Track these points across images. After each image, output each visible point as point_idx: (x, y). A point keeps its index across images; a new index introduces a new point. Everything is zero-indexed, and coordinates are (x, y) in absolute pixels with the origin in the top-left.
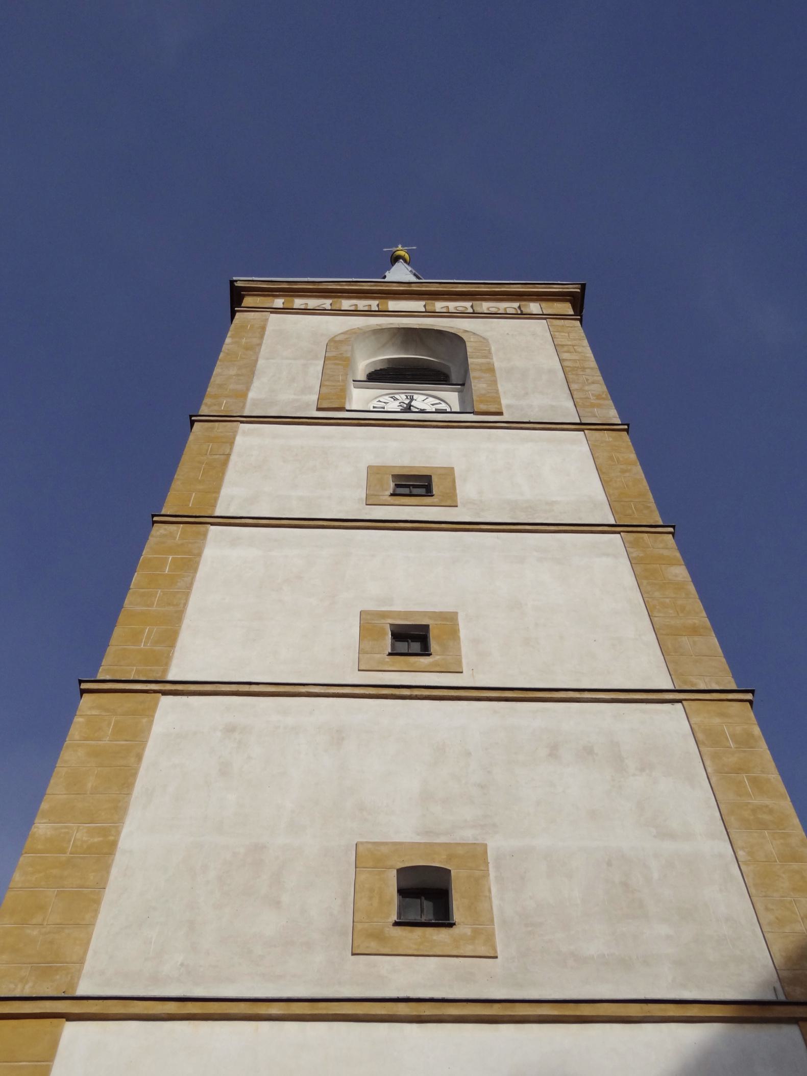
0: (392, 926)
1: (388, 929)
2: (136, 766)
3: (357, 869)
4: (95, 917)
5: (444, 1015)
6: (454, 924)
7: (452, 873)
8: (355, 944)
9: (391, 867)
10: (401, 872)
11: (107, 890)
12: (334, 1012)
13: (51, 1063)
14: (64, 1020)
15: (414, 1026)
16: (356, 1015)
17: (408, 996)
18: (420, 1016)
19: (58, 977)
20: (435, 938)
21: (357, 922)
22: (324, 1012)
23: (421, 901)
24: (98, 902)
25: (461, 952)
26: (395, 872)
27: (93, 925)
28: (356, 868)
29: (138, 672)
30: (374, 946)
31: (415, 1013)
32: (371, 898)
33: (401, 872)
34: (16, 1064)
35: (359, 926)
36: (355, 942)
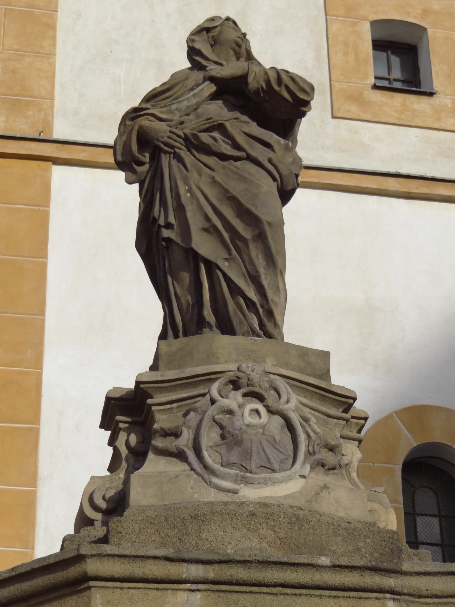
0: (370, 89)
1: (367, 92)
2: (250, 370)
3: (327, 17)
4: (54, 45)
5: (433, 194)
6: (434, 94)
7: (430, 32)
8: (335, 107)
9: (364, 19)
10: (374, 23)
11: (59, 13)
12: (325, 182)
13: (48, 209)
14: (51, 163)
15: (403, 201)
16: (348, 186)
17: (398, 171)
18: (410, 193)
19: (30, 113)
20: (415, 107)
21: (333, 81)
22: (315, 180)
23: (388, 55)
24: (52, 27)
25: (443, 125)
26: (368, 25)
27: (53, 54)
28: (326, 15)
29: (236, 603)
30: (354, 109)
31: (405, 190)
32: (346, 54)
33: (374, 23)
34: (11, 206)
35: (337, 86)
36: (335, 104)
